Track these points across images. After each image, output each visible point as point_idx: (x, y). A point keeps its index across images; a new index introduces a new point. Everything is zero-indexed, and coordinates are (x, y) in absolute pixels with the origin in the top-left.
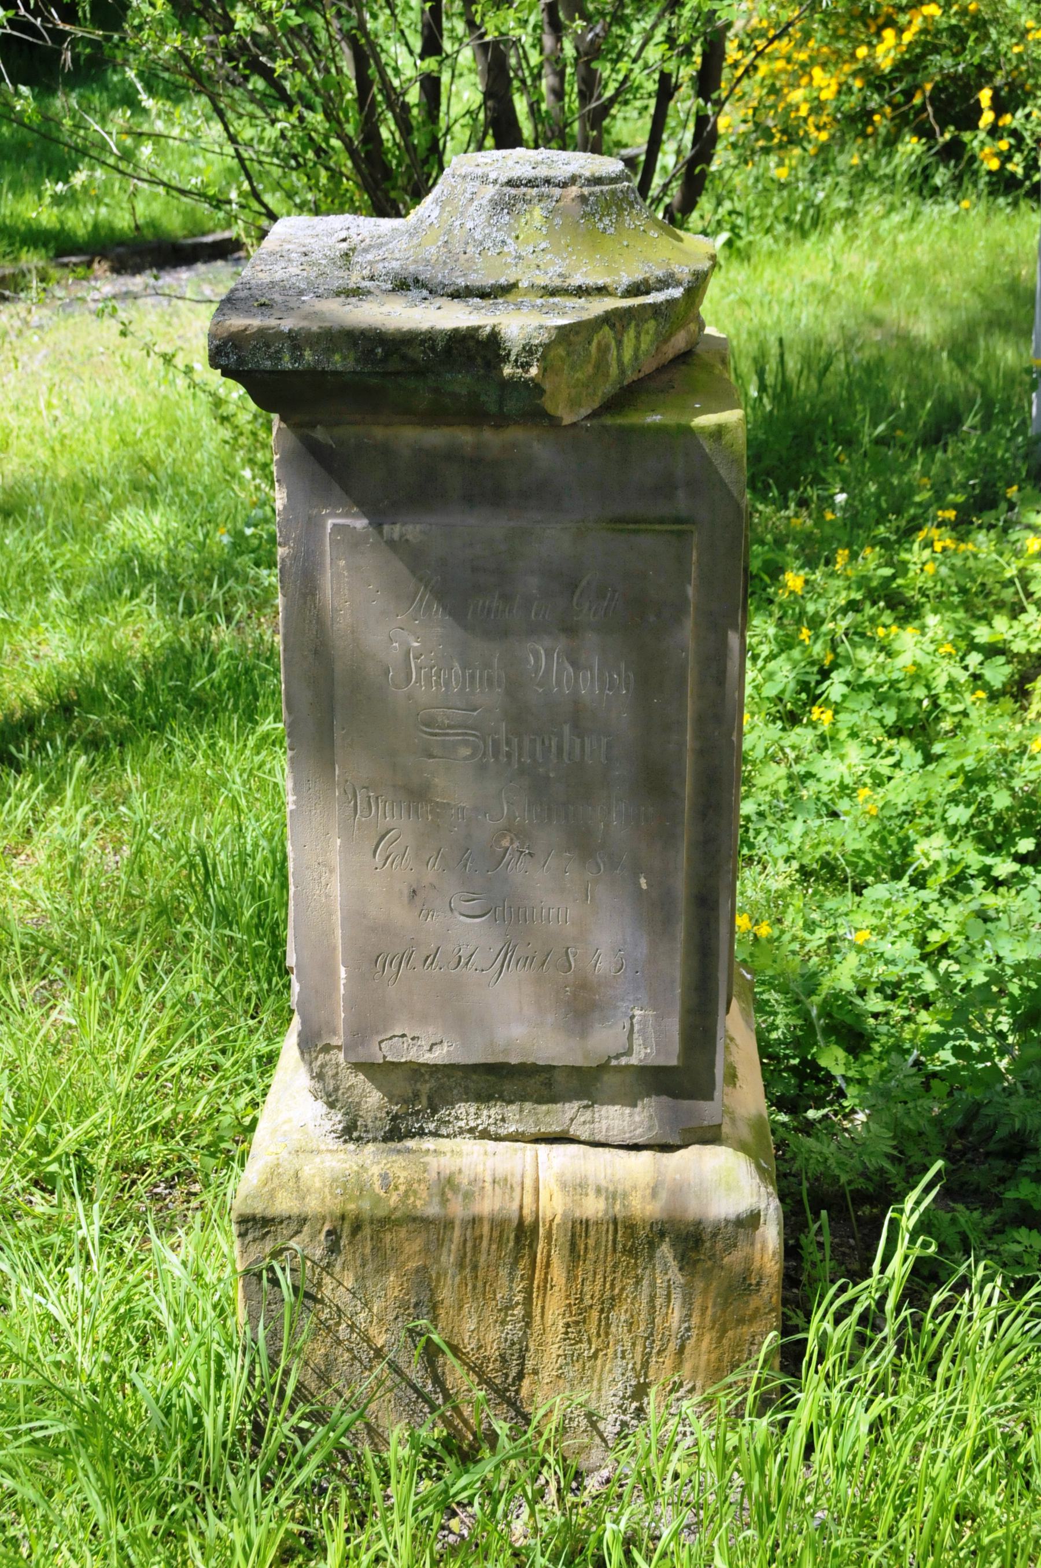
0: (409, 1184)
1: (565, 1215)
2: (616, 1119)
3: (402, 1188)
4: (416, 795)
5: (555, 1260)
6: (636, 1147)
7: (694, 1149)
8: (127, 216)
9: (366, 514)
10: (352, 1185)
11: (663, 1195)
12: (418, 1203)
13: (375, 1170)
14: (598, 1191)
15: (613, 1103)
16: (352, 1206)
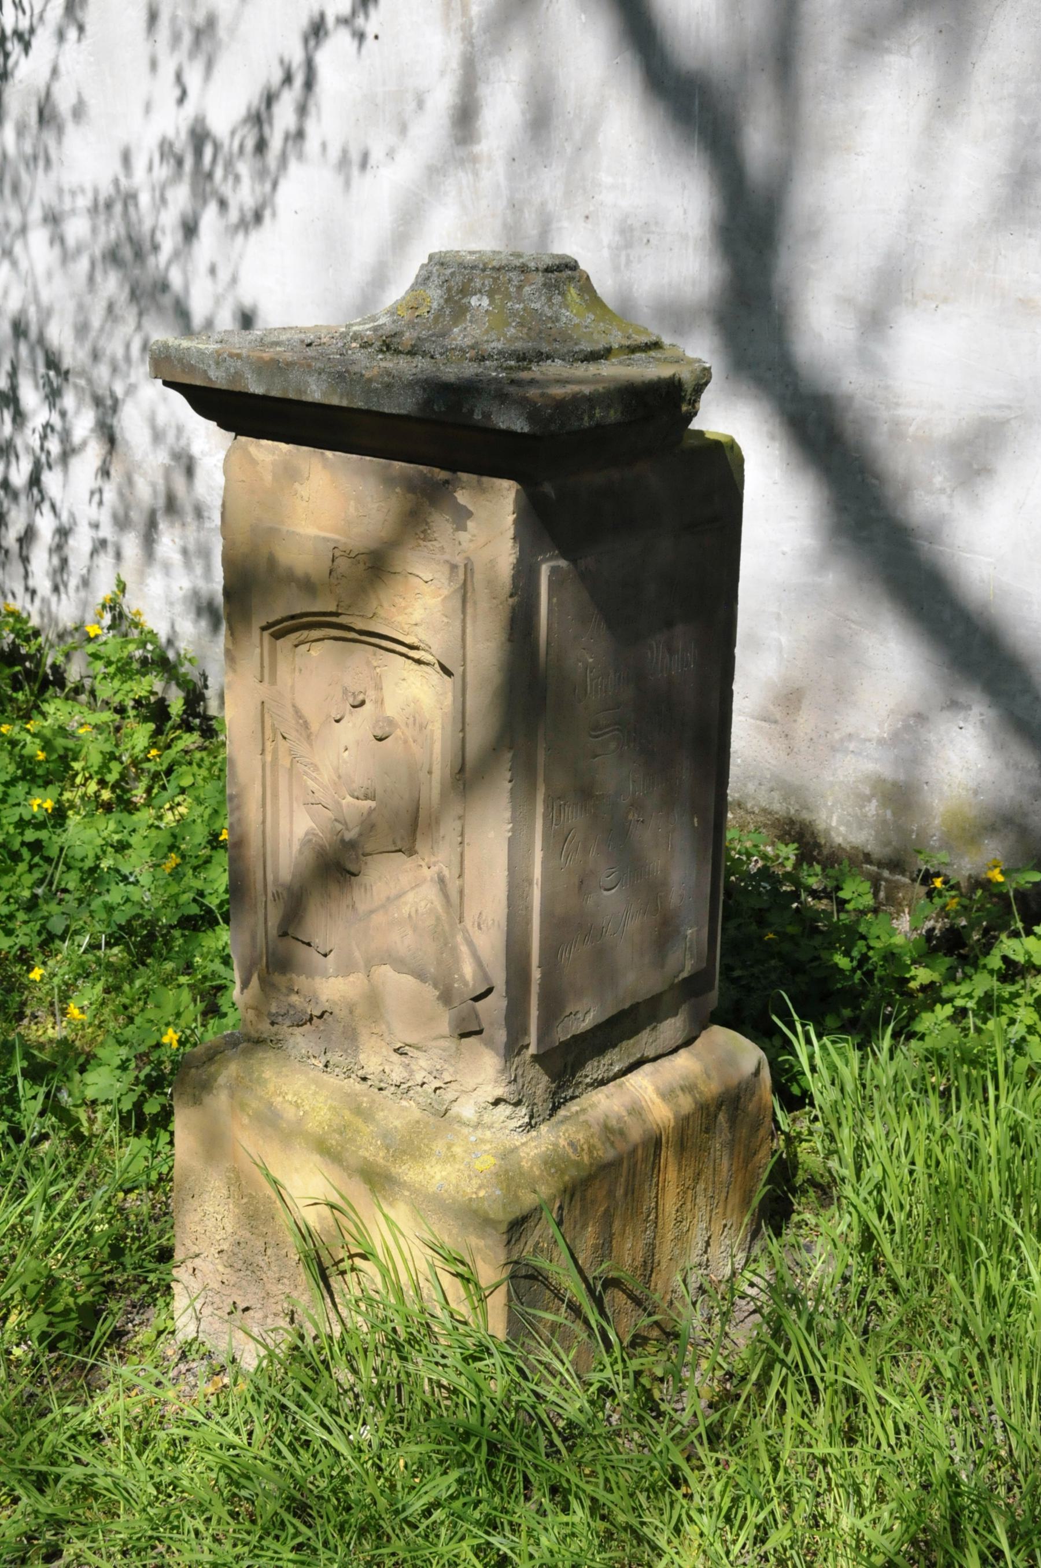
0: (587, 1142)
1: (675, 1118)
2: (671, 1028)
3: (585, 1147)
4: (585, 794)
5: (670, 1160)
6: (675, 1051)
7: (704, 1033)
8: (110, 693)
9: (564, 555)
10: (553, 1162)
11: (714, 1074)
12: (601, 1153)
13: (562, 1142)
14: (682, 1089)
15: (666, 1018)
16: (567, 1178)
